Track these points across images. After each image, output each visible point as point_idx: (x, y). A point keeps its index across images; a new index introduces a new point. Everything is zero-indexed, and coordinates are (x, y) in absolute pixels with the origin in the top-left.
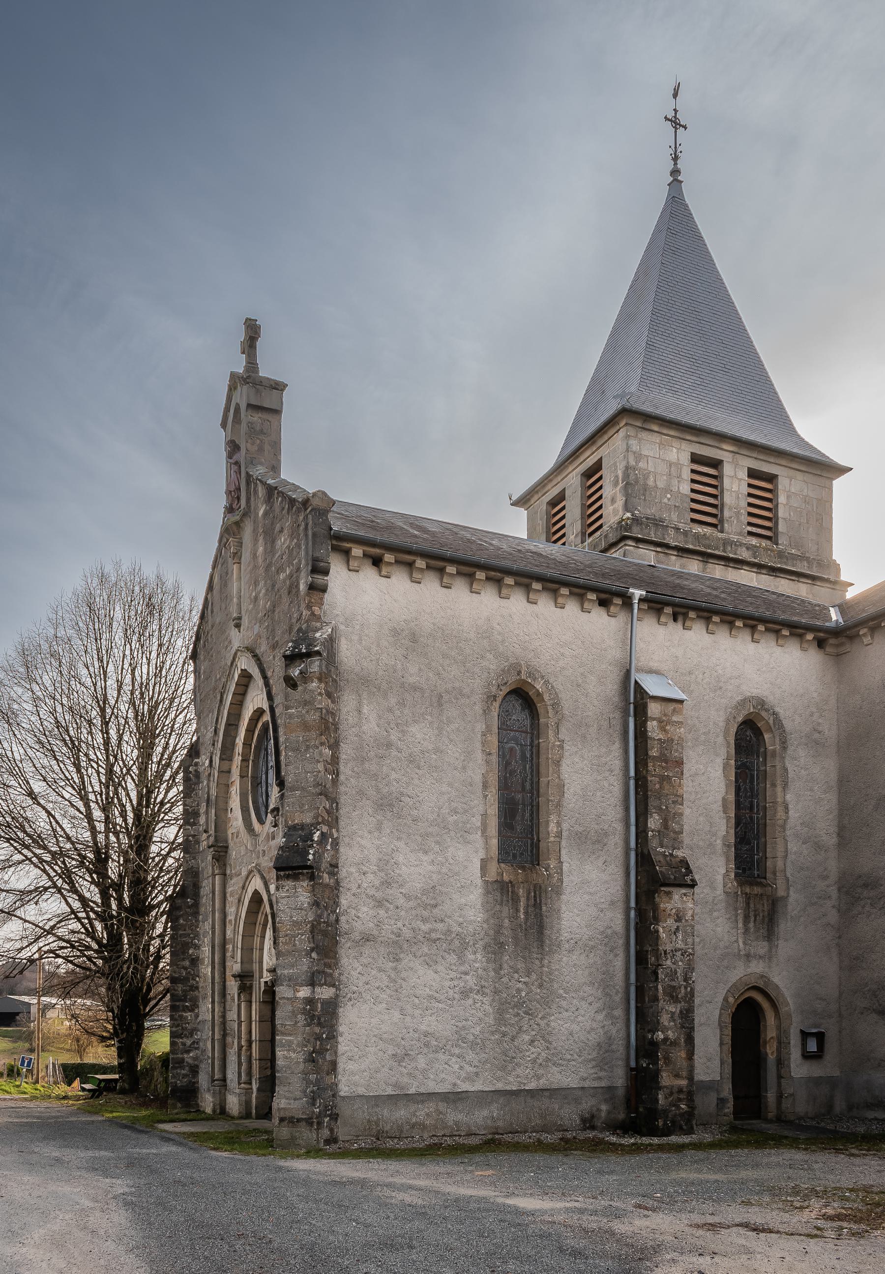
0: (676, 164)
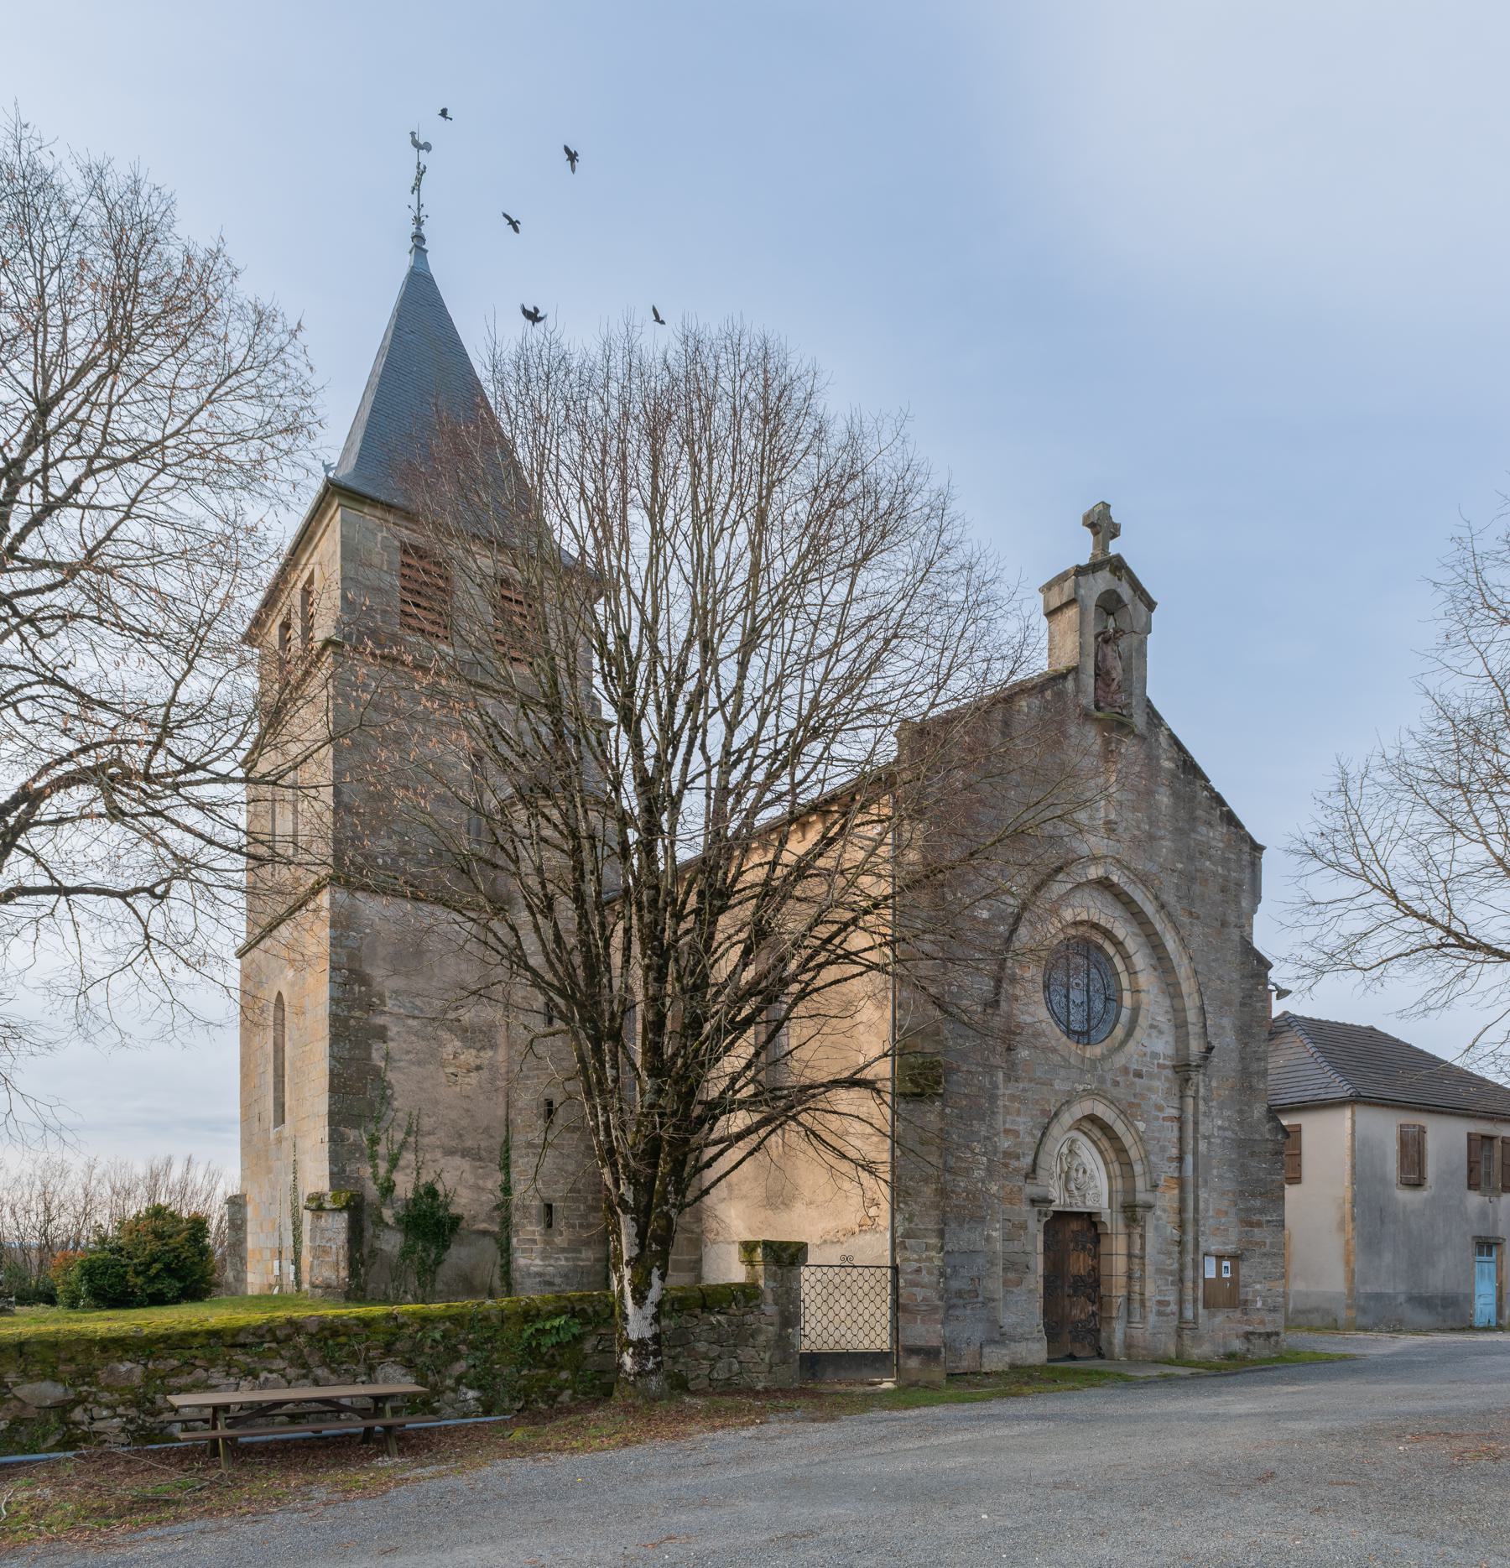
0: (418, 228)
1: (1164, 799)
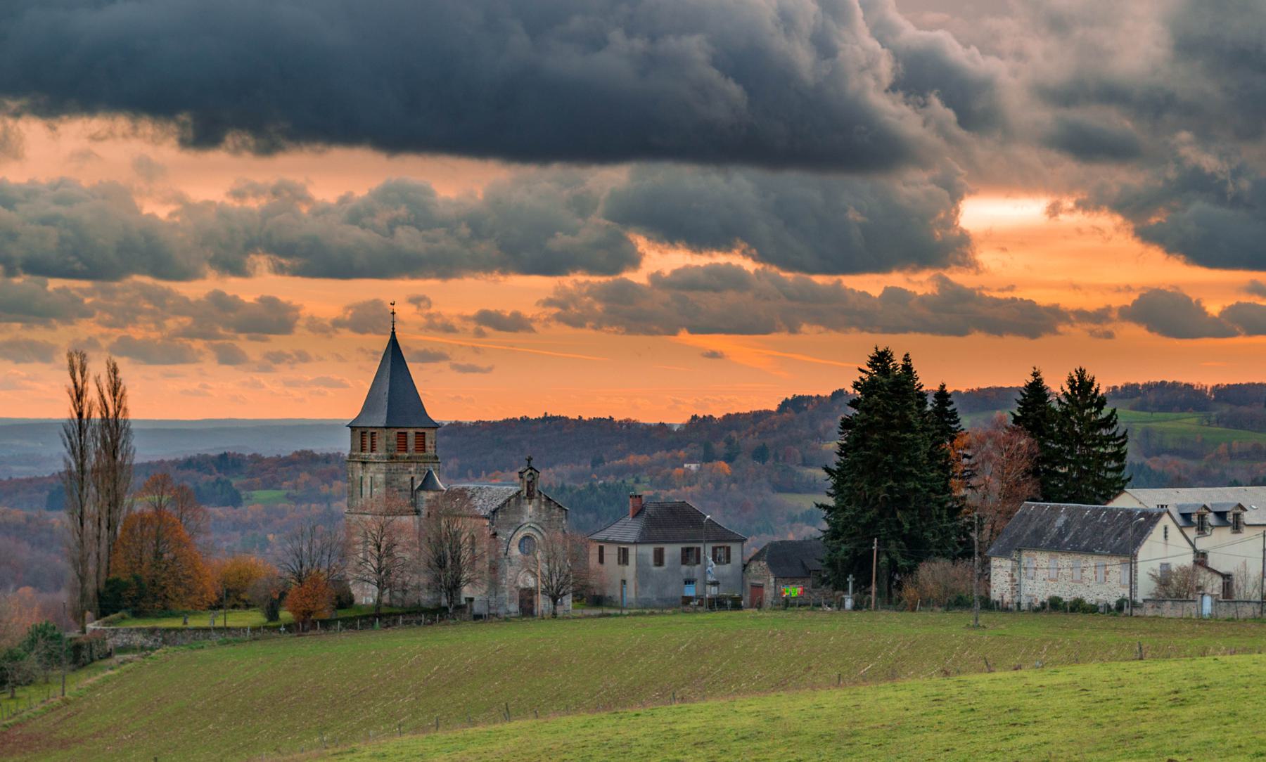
1: (543, 507)
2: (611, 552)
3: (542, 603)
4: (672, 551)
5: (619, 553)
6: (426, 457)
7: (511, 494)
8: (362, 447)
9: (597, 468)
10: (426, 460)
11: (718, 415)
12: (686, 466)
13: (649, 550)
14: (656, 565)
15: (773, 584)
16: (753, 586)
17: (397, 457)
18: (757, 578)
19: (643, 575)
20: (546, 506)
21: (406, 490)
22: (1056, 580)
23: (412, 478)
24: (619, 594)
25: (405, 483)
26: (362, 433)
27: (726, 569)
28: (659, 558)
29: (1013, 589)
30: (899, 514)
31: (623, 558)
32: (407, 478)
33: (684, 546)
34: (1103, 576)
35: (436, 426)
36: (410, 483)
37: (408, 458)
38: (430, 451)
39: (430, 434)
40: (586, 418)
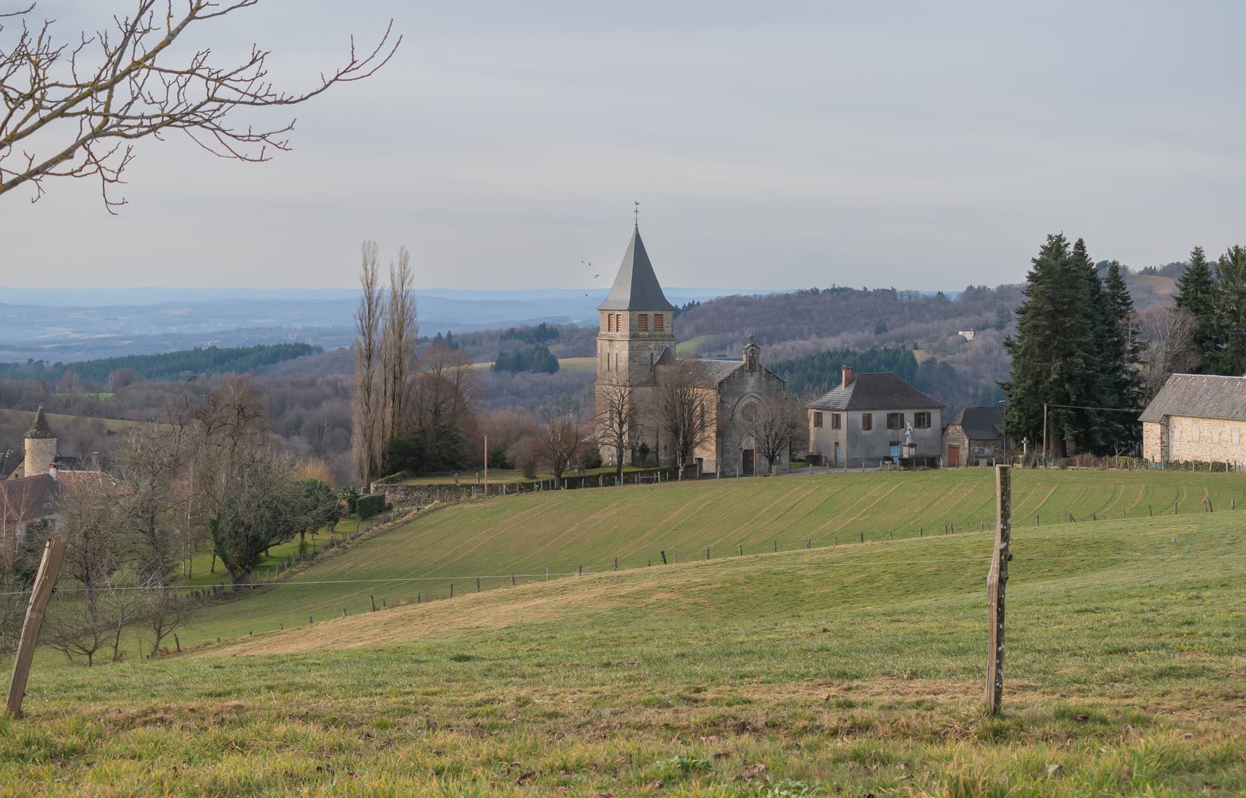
2: (827, 417)
3: (760, 461)
4: (879, 416)
5: (833, 419)
6: (663, 336)
7: (735, 367)
8: (609, 327)
9: (879, 335)
10: (663, 338)
11: (993, 286)
12: (960, 333)
13: (858, 416)
14: (865, 429)
15: (967, 446)
16: (951, 447)
17: (639, 336)
18: (954, 440)
19: (853, 438)
20: (766, 377)
21: (647, 365)
22: (1198, 442)
23: (652, 354)
24: (833, 454)
25: (645, 358)
26: (610, 315)
27: (926, 432)
28: (867, 423)
29: (1162, 450)
30: (1067, 386)
31: (836, 423)
32: (647, 354)
33: (917, 411)
34: (1238, 438)
35: (676, 311)
36: (649, 358)
37: (649, 337)
38: (668, 330)
39: (668, 316)
40: (870, 289)
